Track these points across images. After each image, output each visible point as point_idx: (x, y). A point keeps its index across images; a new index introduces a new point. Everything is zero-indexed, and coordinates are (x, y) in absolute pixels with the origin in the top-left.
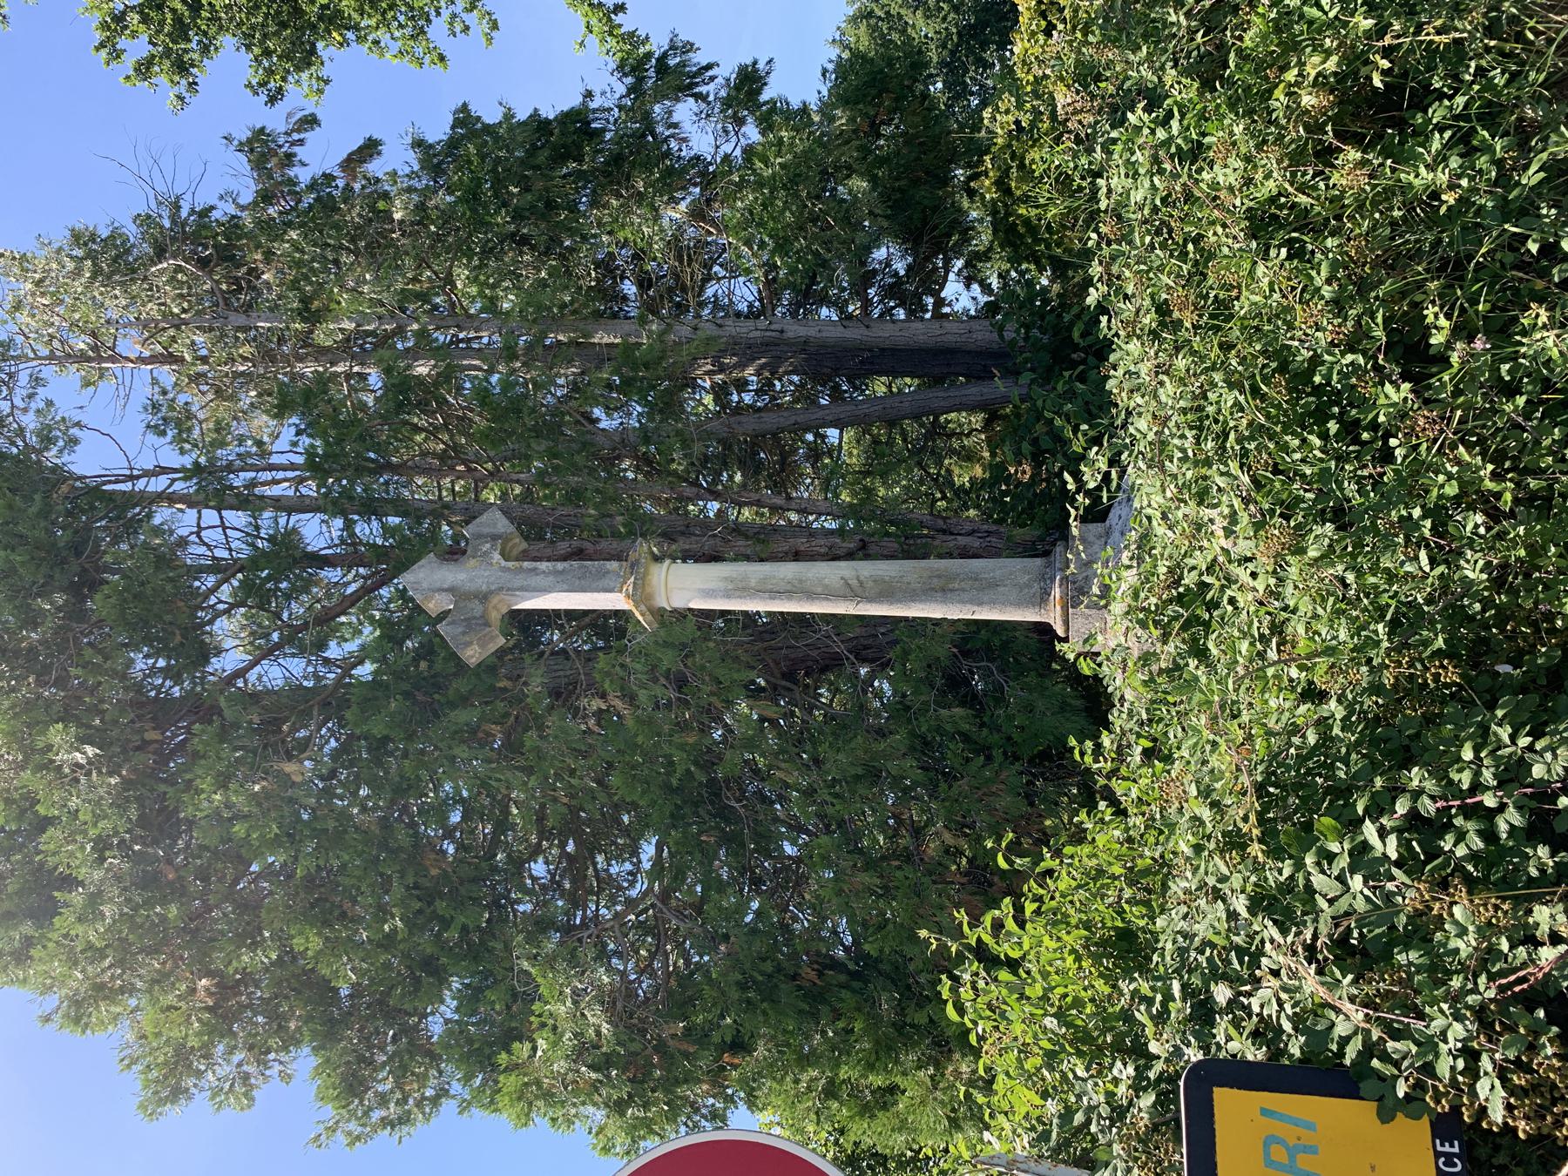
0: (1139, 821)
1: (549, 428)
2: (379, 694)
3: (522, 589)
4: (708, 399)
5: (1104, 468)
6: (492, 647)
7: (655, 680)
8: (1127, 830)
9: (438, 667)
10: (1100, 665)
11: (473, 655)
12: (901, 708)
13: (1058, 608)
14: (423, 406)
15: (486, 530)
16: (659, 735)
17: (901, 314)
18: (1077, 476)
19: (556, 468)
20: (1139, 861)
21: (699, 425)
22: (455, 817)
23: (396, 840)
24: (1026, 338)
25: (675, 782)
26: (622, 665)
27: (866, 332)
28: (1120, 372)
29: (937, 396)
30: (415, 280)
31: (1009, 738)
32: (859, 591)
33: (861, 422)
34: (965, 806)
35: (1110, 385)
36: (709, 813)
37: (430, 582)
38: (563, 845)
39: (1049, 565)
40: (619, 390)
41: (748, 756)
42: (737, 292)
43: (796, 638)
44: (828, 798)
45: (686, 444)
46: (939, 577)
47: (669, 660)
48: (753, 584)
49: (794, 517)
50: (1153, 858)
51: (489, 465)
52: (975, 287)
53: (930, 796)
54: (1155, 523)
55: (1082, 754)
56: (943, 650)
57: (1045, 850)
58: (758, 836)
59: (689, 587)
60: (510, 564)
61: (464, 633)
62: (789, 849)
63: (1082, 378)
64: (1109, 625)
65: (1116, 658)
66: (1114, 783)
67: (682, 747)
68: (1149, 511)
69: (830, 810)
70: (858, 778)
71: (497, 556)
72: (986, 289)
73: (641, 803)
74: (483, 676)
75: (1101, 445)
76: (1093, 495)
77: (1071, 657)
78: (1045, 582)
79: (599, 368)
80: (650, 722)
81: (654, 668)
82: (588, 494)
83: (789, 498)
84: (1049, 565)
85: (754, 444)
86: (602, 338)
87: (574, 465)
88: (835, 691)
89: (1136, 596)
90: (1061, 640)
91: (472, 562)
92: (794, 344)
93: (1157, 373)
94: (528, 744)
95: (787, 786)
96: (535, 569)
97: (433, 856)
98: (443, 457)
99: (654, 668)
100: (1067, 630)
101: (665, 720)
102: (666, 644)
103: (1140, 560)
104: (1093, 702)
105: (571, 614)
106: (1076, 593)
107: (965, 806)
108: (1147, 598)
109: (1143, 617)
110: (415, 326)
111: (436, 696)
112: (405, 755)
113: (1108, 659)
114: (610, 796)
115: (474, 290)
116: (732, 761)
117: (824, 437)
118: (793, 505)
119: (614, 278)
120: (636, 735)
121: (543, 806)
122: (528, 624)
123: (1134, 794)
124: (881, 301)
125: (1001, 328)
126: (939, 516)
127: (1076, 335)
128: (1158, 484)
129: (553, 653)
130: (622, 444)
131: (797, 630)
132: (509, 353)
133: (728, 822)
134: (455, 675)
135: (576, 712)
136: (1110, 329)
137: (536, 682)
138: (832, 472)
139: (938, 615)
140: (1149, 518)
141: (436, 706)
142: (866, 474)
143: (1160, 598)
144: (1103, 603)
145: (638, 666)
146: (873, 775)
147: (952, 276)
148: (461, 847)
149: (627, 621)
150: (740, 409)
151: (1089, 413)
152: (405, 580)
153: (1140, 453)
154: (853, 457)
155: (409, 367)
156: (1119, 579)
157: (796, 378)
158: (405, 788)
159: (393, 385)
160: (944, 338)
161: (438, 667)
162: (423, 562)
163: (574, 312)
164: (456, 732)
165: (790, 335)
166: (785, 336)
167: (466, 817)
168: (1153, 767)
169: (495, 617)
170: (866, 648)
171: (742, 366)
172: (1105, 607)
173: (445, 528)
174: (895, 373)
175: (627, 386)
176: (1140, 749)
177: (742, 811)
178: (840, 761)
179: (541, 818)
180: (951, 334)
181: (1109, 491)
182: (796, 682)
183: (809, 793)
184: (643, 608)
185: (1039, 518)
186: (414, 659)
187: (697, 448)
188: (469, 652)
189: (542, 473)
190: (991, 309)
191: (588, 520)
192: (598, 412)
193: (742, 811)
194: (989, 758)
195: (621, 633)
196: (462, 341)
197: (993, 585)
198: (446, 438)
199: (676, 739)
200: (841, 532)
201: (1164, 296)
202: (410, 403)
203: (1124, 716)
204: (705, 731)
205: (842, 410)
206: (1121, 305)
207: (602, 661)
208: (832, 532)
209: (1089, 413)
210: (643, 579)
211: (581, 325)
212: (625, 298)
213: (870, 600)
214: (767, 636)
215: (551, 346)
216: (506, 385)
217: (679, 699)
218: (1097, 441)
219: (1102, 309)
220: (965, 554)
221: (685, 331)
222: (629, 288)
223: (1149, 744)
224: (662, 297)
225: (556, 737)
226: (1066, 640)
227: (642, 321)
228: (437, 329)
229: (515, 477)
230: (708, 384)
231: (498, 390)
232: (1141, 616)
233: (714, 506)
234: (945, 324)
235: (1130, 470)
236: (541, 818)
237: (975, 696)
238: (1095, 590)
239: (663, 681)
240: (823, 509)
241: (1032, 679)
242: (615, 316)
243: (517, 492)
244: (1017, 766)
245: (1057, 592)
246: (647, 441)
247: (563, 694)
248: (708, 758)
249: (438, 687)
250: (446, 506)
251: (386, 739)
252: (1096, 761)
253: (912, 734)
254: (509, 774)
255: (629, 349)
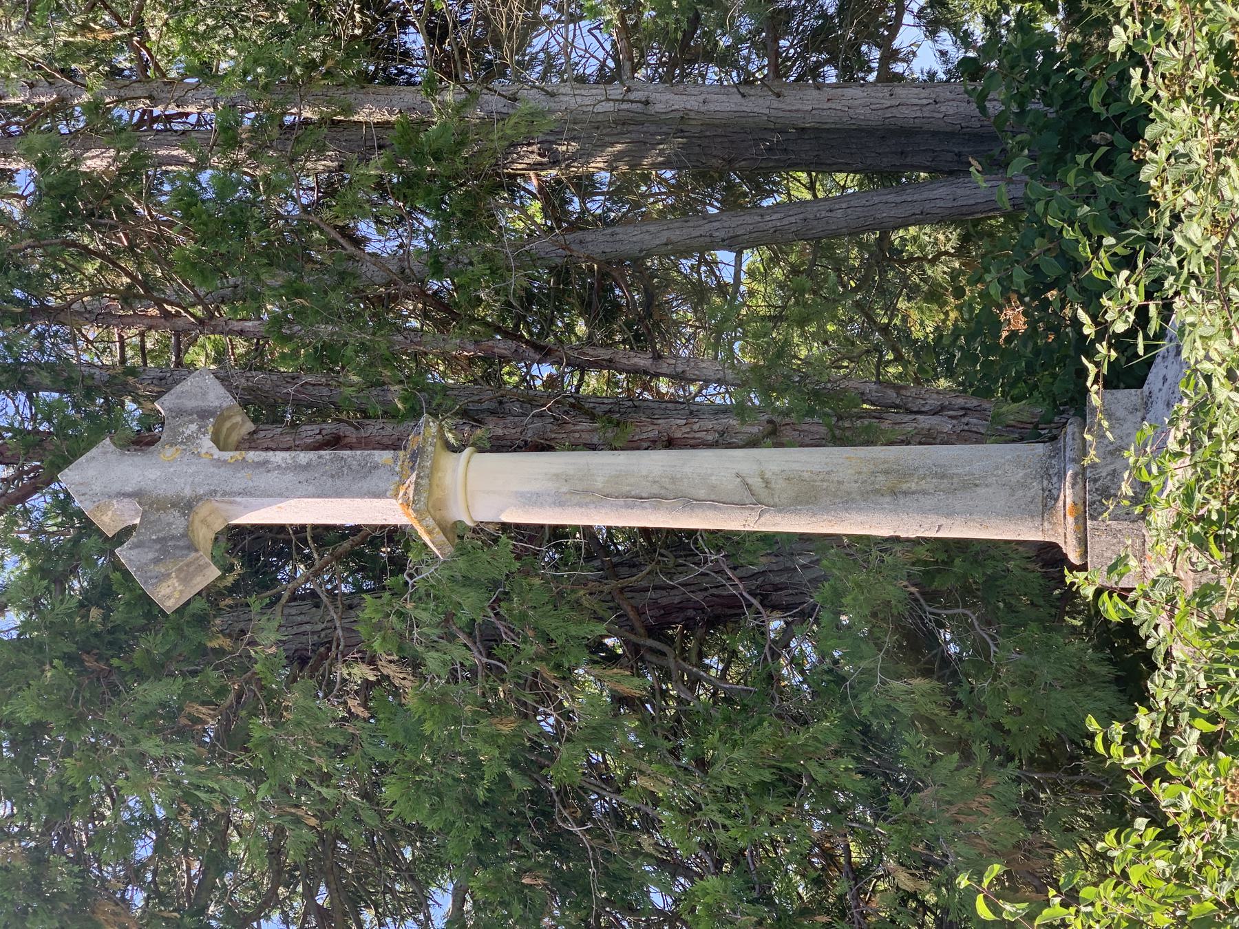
0: (1194, 845)
1: (289, 252)
2: (27, 658)
3: (244, 493)
4: (535, 207)
5: (1138, 300)
6: (200, 583)
7: (451, 638)
8: (1177, 859)
9: (117, 616)
10: (1133, 605)
11: (170, 594)
12: (831, 683)
13: (1070, 519)
14: (94, 218)
15: (190, 404)
16: (457, 721)
17: (831, 74)
18: (1097, 315)
19: (300, 313)
20: (1194, 906)
21: (518, 245)
22: (144, 850)
23: (53, 883)
24: (1023, 112)
25: (481, 794)
26: (401, 615)
27: (776, 104)
28: (1163, 153)
29: (886, 202)
30: (84, 27)
31: (998, 726)
32: (763, 494)
33: (775, 241)
34: (929, 830)
35: (1147, 173)
36: (535, 842)
37: (104, 483)
38: (310, 893)
39: (1057, 453)
40: (396, 192)
41: (596, 757)
42: (579, 43)
43: (670, 575)
44: (720, 819)
45: (495, 272)
46: (886, 472)
47: (471, 605)
48: (599, 485)
49: (664, 386)
50: (1218, 903)
51: (198, 311)
52: (945, 35)
53: (876, 817)
54: (1215, 384)
55: (1107, 743)
56: (896, 590)
57: (1052, 892)
58: (612, 878)
59: (502, 489)
60: (227, 455)
61: (157, 561)
62: (657, 899)
63: (1106, 165)
64: (1148, 545)
65: (1158, 594)
66: (1157, 787)
67: (492, 739)
68: (1207, 366)
69: (721, 836)
70: (764, 787)
71: (206, 443)
72: (965, 39)
73: (430, 826)
74: (188, 631)
75: (1133, 268)
76: (1123, 343)
77: (1089, 592)
78: (1051, 476)
79: (365, 160)
80: (440, 701)
81: (449, 618)
82: (349, 352)
83: (658, 357)
84: (1057, 453)
85: (604, 275)
86: (369, 113)
87: (326, 307)
88: (731, 657)
89: (1188, 498)
90: (1072, 568)
91: (169, 452)
92: (665, 122)
93: (1218, 156)
94: (256, 734)
95: (656, 802)
96: (266, 462)
97: (109, 908)
98: (127, 297)
99: (449, 618)
100: (1085, 554)
101: (466, 699)
102: (467, 581)
103: (1196, 444)
104: (1125, 662)
105: (324, 535)
106: (1097, 496)
107: (929, 830)
108: (1206, 502)
109: (1202, 532)
110: (86, 97)
111: (115, 662)
112: (68, 752)
113: (1146, 596)
114: (382, 816)
115: (175, 43)
116: (569, 765)
117: (712, 265)
118: (664, 369)
119: (389, 24)
120: (421, 721)
121: (280, 832)
122: (258, 549)
123: (1187, 802)
124: (801, 56)
125: (982, 98)
126: (888, 384)
127: (1095, 100)
128: (1219, 322)
129: (294, 598)
130: (405, 278)
131: (670, 561)
132: (228, 137)
133: (564, 856)
134: (143, 629)
135: (329, 686)
136: (1145, 87)
137: (268, 639)
138: (725, 319)
139: (885, 532)
140: (1208, 379)
141: (114, 678)
142: (776, 319)
143: (1225, 501)
144: (1138, 510)
145: (424, 616)
146: (787, 783)
147: (908, 19)
148: (154, 894)
149: (407, 548)
150: (581, 223)
151: (1115, 218)
152: (69, 478)
153: (1192, 275)
154: (761, 298)
155: (76, 160)
156: (1162, 472)
157: (668, 174)
158: (63, 804)
159: (50, 187)
160: (895, 112)
161: (117, 616)
162: (94, 452)
163: (328, 74)
164: (146, 717)
165: (660, 107)
166: (652, 109)
167: (160, 848)
168: (1217, 760)
169: (204, 536)
170: (777, 588)
171: (585, 155)
172: (1143, 516)
173: (130, 405)
174: (820, 165)
175: (409, 187)
176: (1195, 735)
177: (586, 839)
178: (735, 763)
179: (276, 853)
180: (907, 107)
181: (1146, 337)
182: (670, 641)
183: (690, 811)
184: (430, 522)
185: (1043, 382)
186: (81, 605)
187: (516, 281)
188: (106, 519)
189: (278, 321)
190: (970, 69)
191: (349, 391)
192: (365, 228)
193: (586, 839)
194: (967, 757)
195: (398, 564)
196: (157, 119)
197: (969, 484)
198: (131, 267)
199: (484, 726)
200: (740, 410)
201: (1228, 37)
202: (77, 213)
203: (1172, 684)
204: (527, 715)
205: (739, 223)
206: (1162, 51)
207: (370, 608)
208: (723, 410)
209: (1115, 218)
210: (430, 477)
211: (338, 93)
212: (406, 54)
213: (780, 508)
214: (623, 570)
215: (292, 127)
216: (225, 186)
217: (489, 667)
218: (1128, 262)
219: (1133, 56)
220: (929, 438)
221: (493, 102)
222: (415, 40)
223: (1209, 728)
224: (462, 52)
225: (298, 724)
226: (1083, 568)
227: (432, 86)
228: (120, 100)
229: (237, 326)
230: (533, 186)
231: (210, 195)
232: (1197, 529)
233: (547, 370)
234: (899, 90)
235: (1178, 303)
236: (276, 853)
237: (946, 660)
238: (1126, 489)
239: (462, 638)
240: (709, 373)
241: (1033, 632)
242: (390, 81)
243: (241, 350)
244: (1011, 769)
245: (1068, 495)
246: (438, 270)
247: (307, 659)
248: (533, 757)
249: (117, 647)
250: (132, 371)
251: (39, 727)
252: (1129, 753)
253: (848, 720)
254: (226, 782)
255: (412, 128)
